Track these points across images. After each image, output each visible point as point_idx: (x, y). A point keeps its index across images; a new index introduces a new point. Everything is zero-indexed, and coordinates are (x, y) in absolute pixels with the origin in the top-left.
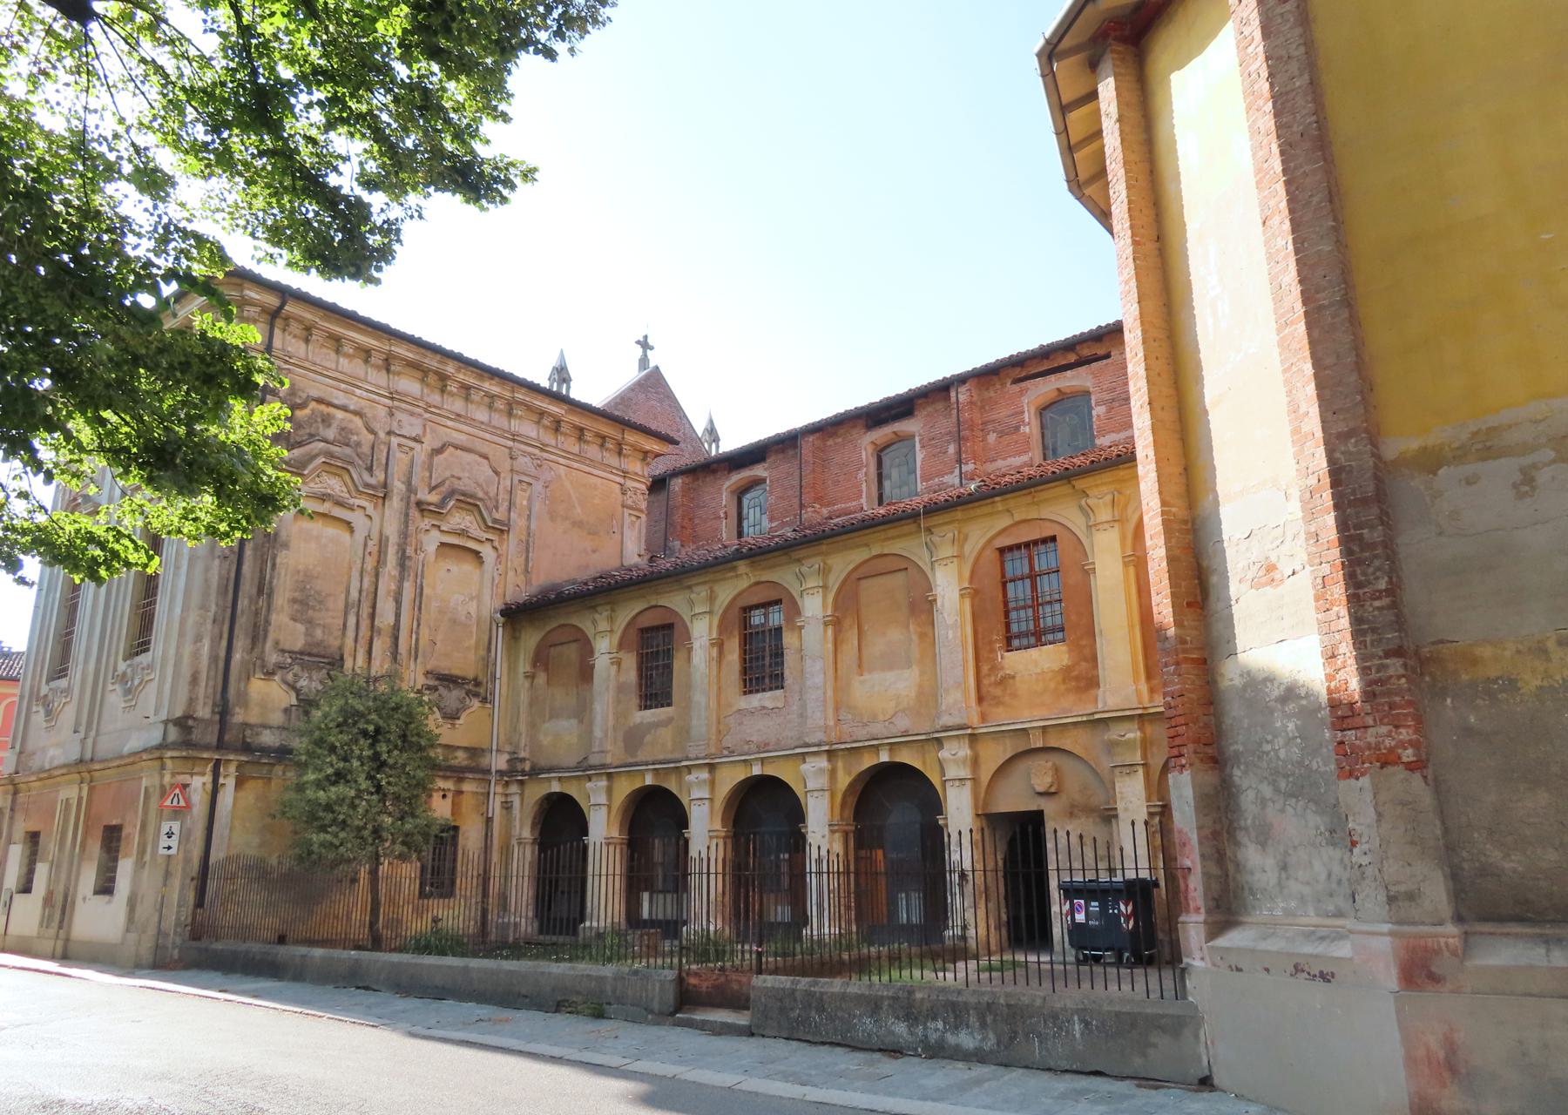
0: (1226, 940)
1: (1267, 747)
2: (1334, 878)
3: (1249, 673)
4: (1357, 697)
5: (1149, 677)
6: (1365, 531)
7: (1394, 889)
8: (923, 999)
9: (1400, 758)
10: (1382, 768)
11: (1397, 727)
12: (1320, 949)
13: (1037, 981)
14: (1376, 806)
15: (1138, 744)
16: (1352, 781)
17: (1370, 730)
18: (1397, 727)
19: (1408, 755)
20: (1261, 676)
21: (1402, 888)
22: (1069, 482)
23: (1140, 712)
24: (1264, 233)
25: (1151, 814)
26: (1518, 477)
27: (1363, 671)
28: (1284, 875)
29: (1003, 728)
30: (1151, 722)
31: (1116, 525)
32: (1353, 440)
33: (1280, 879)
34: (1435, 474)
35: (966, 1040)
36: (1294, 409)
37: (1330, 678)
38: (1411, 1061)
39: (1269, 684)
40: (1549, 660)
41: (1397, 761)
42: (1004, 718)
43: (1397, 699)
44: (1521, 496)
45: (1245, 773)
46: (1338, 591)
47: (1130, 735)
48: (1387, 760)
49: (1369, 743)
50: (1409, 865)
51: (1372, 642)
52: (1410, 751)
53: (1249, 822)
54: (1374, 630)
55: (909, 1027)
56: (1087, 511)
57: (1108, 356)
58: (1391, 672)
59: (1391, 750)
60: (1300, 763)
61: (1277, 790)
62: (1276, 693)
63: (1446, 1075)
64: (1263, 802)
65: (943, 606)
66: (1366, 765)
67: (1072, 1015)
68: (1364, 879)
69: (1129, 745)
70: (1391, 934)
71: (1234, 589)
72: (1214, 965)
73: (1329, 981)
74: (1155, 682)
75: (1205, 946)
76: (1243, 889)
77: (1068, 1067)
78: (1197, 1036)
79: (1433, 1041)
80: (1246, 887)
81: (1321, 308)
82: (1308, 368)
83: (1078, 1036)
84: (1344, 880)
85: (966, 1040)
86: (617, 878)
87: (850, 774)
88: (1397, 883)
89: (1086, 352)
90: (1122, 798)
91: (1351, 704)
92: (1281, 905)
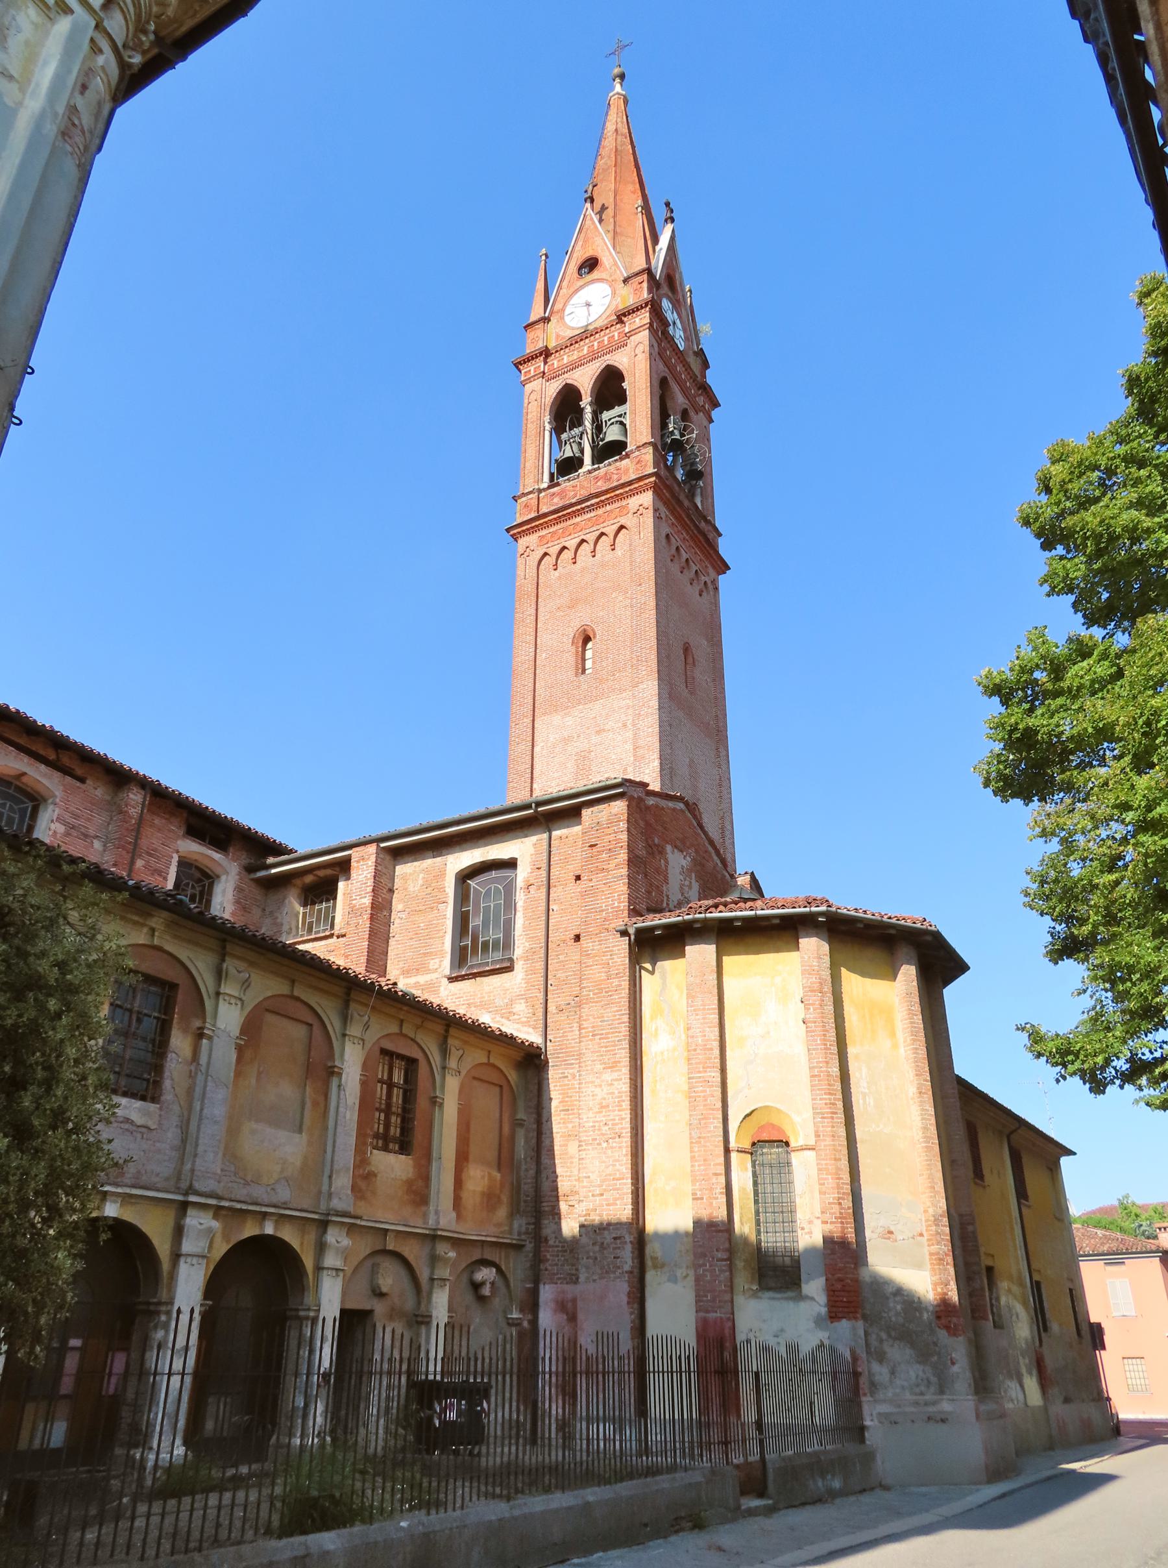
1: (885, 1315)
3: (875, 1277)
20: (882, 1281)
29: (377, 1225)
57: (82, 780)
60: (903, 1325)
61: (889, 1336)
62: (890, 1290)
64: (881, 1341)
65: (346, 1083)
72: (880, 1422)
86: (632, 1375)
87: (228, 1242)
89: (66, 760)
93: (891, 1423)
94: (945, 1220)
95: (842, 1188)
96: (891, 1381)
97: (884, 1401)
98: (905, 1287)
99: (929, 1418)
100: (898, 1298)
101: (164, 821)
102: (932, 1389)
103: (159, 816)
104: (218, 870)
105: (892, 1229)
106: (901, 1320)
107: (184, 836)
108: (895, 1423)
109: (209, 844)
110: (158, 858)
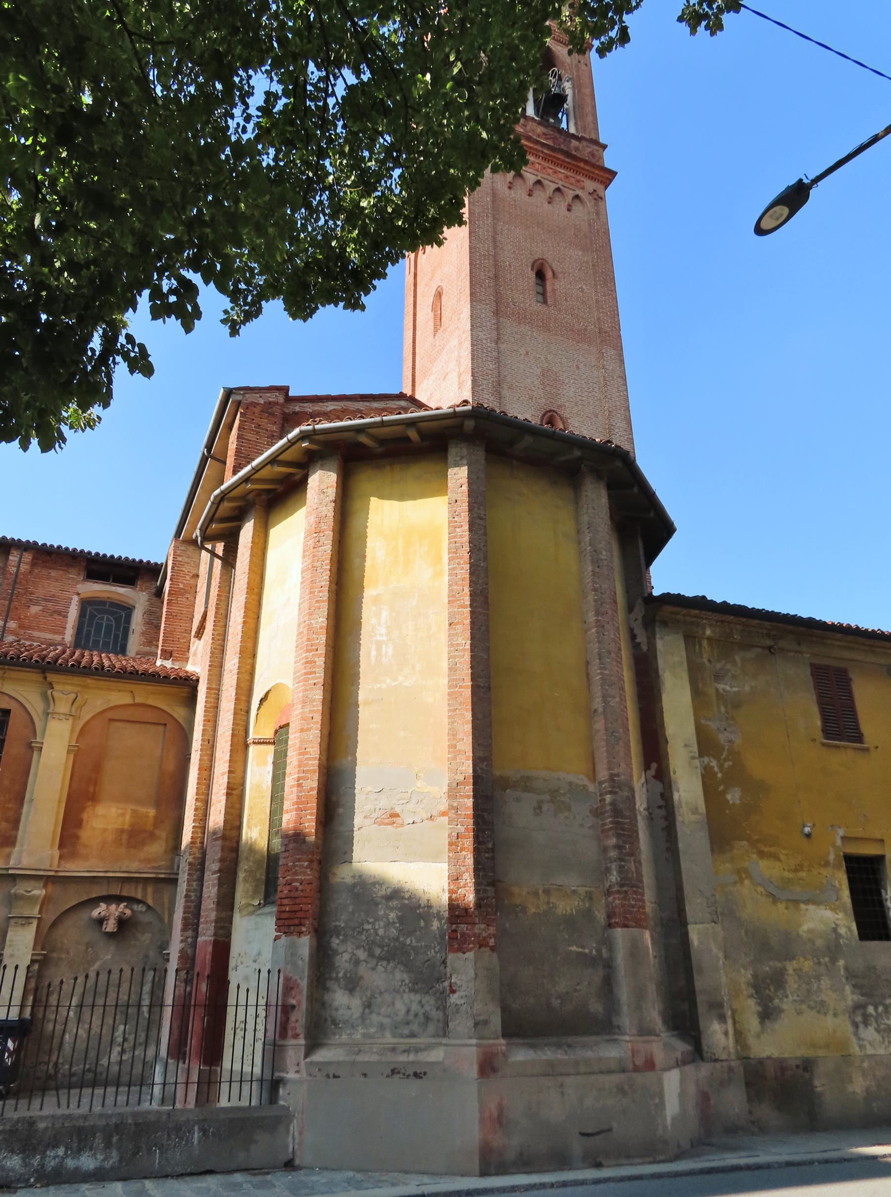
0: (320, 1056)
1: (367, 927)
2: (412, 1013)
3: (360, 876)
4: (472, 905)
5: (61, 846)
6: (485, 814)
7: (477, 1018)
8: (47, 1128)
9: (488, 943)
10: (480, 948)
11: (488, 925)
12: (412, 1057)
13: (76, 1104)
14: (475, 970)
15: (40, 901)
16: (460, 955)
17: (477, 926)
18: (488, 925)
19: (492, 942)
21: (482, 1018)
22: (44, 672)
23: (52, 873)
24: (449, 630)
25: (33, 961)
26: (535, 804)
27: (477, 891)
28: (367, 1011)
30: (53, 883)
31: (71, 718)
32: (485, 763)
33: (363, 1013)
34: (505, 791)
35: (88, 1162)
36: (453, 734)
37: (451, 892)
38: (482, 1121)
39: (377, 886)
40: (539, 899)
41: (486, 945)
42: (76, 868)
43: (490, 910)
44: (536, 814)
45: (344, 941)
46: (468, 843)
47: (36, 892)
48: (482, 944)
49: (475, 933)
50: (486, 1004)
51: (482, 875)
52: (493, 940)
53: (341, 975)
54: (484, 870)
55: (24, 1160)
56: (47, 700)
58: (489, 894)
59: (484, 938)
60: (397, 939)
61: (371, 955)
62: (383, 892)
63: (497, 1126)
64: (357, 962)
66: (471, 946)
67: (194, 1126)
68: (458, 1012)
69: (31, 900)
70: (477, 1045)
71: (358, 820)
73: (421, 1078)
74: (65, 851)
75: (303, 1063)
76: (326, 1020)
77: (184, 1171)
78: (288, 1131)
79: (493, 1106)
80: (329, 1019)
81: (479, 686)
82: (469, 716)
83: (196, 1142)
84: (420, 1013)
85: (88, 1162)
88: (480, 1015)
90: (10, 946)
91: (466, 910)
92: (360, 1031)
93: (328, 1076)
94: (469, 789)
95: (306, 765)
96: (363, 1017)
97: (341, 1045)
98: (407, 886)
99: (393, 1072)
100: (394, 903)
101: (61, 572)
102: (431, 1028)
103: (54, 569)
104: (131, 602)
105: (398, 810)
106: (393, 932)
107: (84, 580)
108: (335, 1076)
109: (113, 582)
110: (56, 602)
